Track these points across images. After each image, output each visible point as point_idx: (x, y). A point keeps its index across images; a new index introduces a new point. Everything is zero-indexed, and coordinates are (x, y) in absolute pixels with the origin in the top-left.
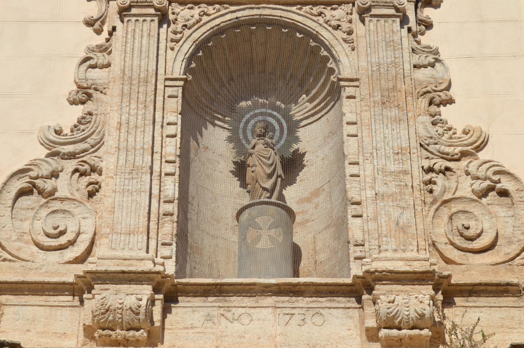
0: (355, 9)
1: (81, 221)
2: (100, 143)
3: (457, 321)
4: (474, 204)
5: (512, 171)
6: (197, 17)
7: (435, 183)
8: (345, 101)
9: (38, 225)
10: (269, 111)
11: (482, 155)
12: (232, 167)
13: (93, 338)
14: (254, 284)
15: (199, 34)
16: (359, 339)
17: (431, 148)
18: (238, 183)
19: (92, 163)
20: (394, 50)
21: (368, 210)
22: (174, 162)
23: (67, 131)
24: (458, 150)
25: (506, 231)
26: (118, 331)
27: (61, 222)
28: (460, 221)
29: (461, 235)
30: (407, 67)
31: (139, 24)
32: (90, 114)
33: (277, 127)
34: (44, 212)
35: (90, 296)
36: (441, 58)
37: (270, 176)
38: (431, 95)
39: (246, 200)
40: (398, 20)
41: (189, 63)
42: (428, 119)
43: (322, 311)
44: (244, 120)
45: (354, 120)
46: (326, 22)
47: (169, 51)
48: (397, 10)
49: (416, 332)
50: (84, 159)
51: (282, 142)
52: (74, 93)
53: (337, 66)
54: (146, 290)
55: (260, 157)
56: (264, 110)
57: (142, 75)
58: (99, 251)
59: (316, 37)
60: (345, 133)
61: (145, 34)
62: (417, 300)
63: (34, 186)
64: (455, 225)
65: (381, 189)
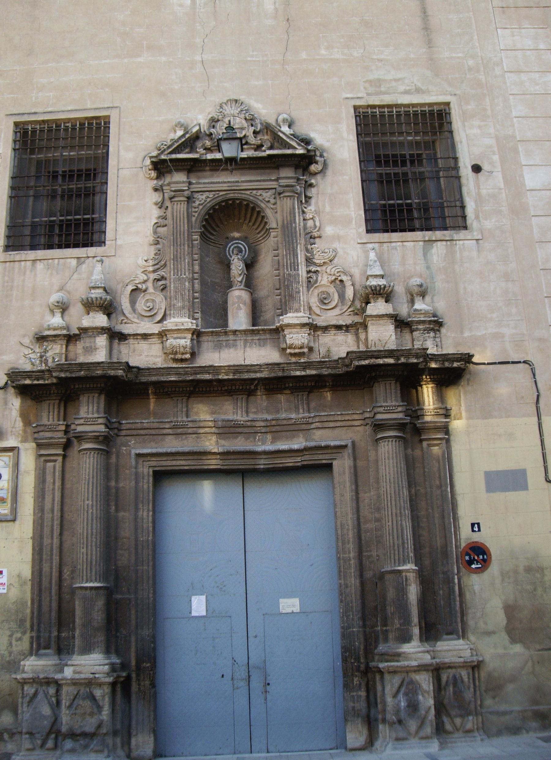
33: (243, 249)
37: (240, 275)
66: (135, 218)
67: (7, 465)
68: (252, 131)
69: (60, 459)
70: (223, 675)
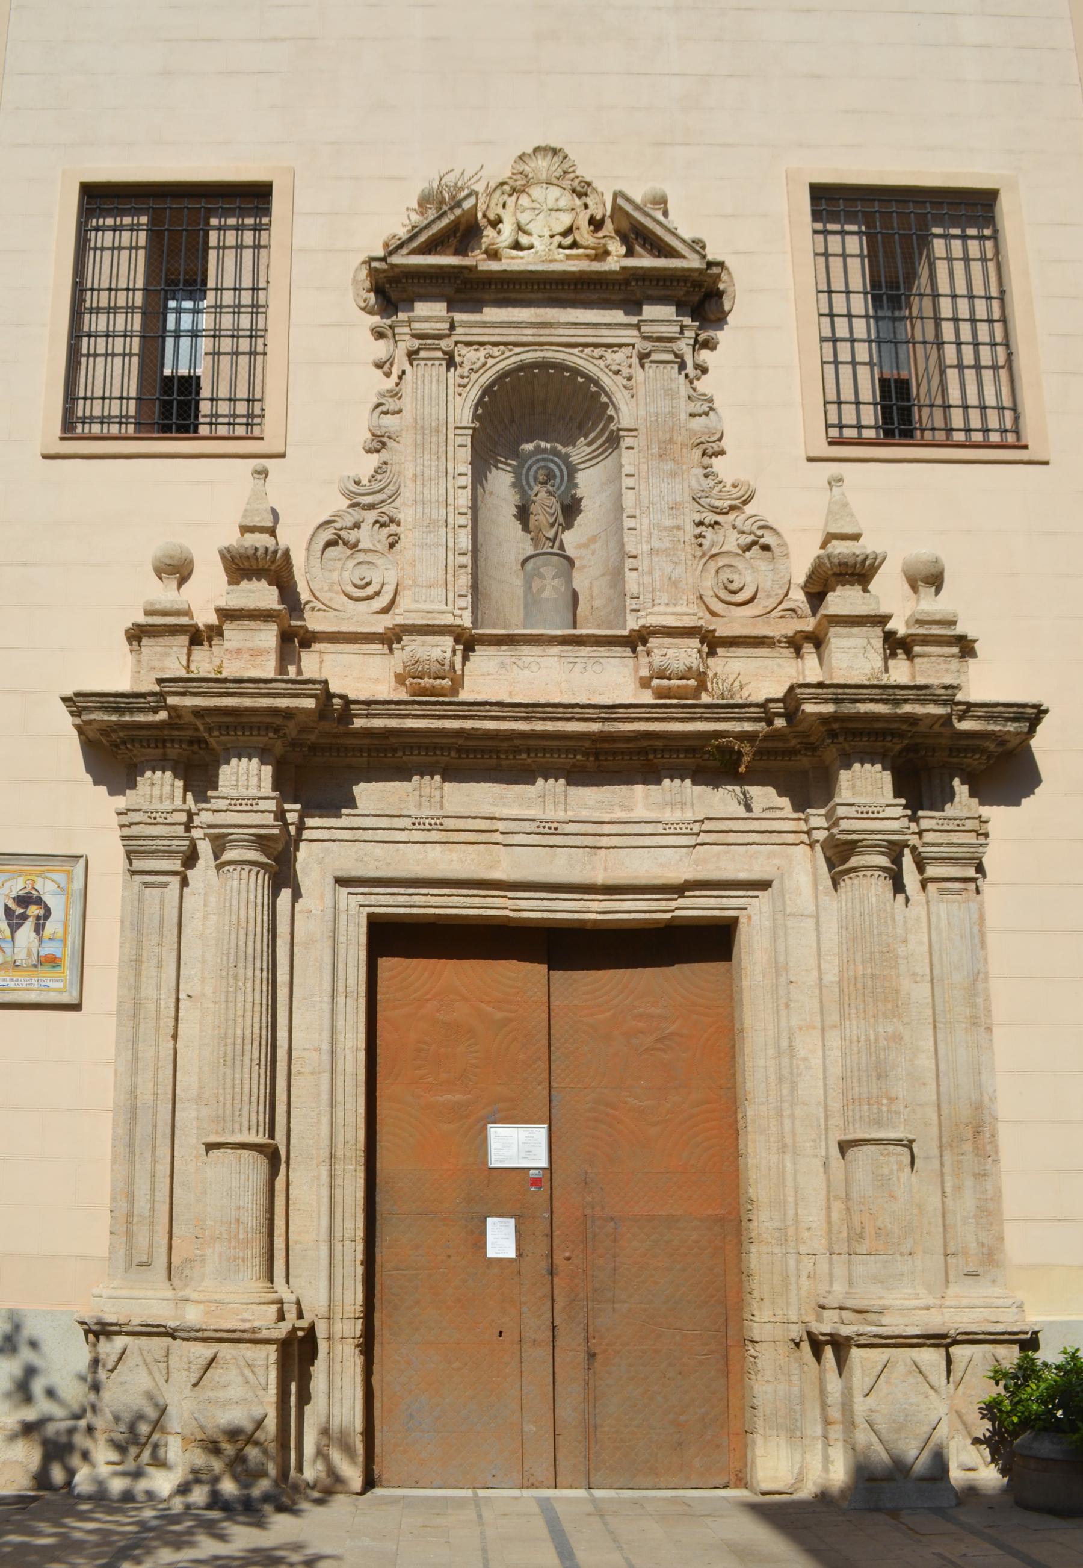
0: (635, 352)
1: (384, 573)
2: (396, 494)
3: (719, 670)
4: (738, 558)
5: (774, 527)
6: (482, 360)
7: (704, 537)
8: (624, 451)
9: (346, 575)
10: (551, 457)
11: (749, 509)
12: (514, 511)
13: (403, 684)
14: (542, 635)
15: (486, 378)
16: (633, 686)
17: (702, 501)
18: (520, 527)
19: (391, 514)
20: (672, 399)
21: (643, 564)
22: (466, 514)
23: (365, 481)
24: (729, 503)
25: (767, 584)
26: (426, 679)
27: (368, 573)
28: (725, 575)
29: (726, 588)
30: (684, 416)
31: (428, 369)
32: (386, 463)
33: (558, 473)
34: (351, 564)
35: (399, 646)
36: (715, 406)
37: (552, 525)
38: (704, 446)
39: (530, 551)
40: (676, 366)
41: (476, 409)
42: (701, 472)
43: (601, 660)
44: (527, 466)
45: (632, 473)
46: (607, 367)
47: (457, 397)
48: (676, 356)
49: (684, 682)
50: (383, 510)
51: (562, 488)
52: (369, 441)
53: (617, 413)
54: (449, 641)
55: (543, 506)
56: (545, 456)
57: (434, 424)
58: (403, 603)
59: (597, 383)
60: (624, 486)
61: (434, 380)
62: (683, 654)
63: (339, 537)
64: (720, 578)
65: (656, 544)
66: (330, 386)
67: (62, 889)
68: (587, 217)
69: (175, 881)
70: (501, 1332)
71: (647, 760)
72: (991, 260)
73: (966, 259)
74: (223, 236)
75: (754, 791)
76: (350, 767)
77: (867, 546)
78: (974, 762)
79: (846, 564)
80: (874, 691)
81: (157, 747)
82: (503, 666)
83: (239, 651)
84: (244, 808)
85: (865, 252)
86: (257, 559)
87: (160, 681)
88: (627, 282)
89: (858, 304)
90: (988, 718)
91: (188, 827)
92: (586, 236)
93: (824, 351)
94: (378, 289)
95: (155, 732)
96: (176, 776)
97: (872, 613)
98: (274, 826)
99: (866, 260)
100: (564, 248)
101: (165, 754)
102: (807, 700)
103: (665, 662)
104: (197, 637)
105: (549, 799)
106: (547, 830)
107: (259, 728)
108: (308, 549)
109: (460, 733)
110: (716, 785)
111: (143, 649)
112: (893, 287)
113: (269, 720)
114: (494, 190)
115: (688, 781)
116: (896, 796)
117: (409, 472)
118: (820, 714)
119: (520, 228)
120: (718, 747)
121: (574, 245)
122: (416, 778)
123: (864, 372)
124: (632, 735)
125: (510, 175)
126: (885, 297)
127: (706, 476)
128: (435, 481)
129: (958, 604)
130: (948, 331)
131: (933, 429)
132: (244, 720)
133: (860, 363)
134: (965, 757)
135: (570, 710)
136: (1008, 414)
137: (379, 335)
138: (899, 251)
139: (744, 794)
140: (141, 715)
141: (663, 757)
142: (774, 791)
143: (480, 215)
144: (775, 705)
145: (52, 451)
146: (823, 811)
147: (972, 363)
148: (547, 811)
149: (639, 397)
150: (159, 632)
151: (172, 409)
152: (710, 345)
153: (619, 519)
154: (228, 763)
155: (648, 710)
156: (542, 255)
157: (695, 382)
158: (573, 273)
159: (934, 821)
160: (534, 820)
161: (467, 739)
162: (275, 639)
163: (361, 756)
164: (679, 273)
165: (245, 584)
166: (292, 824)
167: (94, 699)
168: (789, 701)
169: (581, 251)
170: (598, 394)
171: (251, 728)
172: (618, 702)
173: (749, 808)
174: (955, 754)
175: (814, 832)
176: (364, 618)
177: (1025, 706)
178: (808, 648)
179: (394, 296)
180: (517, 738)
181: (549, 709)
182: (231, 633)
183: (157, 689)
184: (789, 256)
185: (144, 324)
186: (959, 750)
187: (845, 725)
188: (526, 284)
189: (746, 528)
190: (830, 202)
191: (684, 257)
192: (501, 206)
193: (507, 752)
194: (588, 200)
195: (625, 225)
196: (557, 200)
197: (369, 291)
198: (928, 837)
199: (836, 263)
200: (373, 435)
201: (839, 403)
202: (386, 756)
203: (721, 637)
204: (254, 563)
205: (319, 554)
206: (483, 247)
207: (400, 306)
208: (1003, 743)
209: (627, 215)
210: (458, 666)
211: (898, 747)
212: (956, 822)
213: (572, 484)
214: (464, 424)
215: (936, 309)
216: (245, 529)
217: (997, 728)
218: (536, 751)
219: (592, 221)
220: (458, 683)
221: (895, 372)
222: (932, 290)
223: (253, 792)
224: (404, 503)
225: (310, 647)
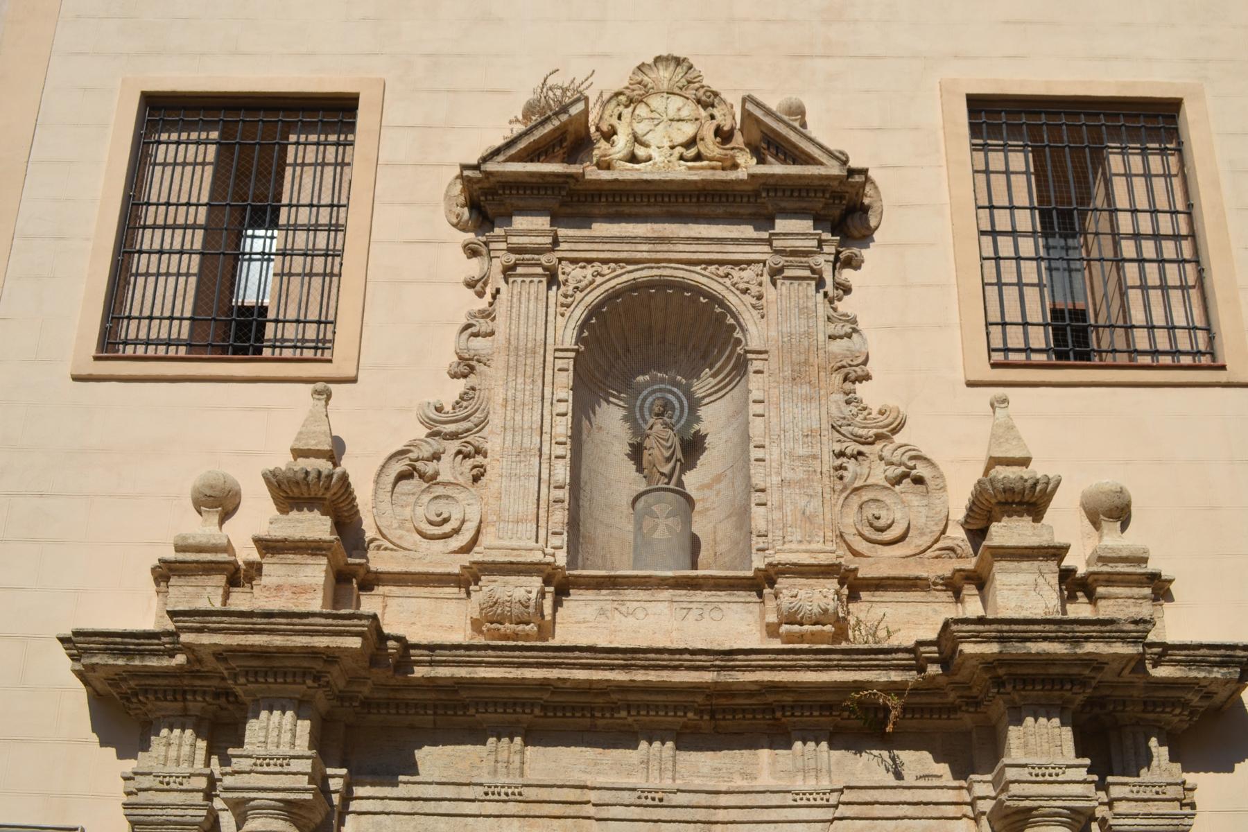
0: (766, 270)
1: (465, 508)
2: (484, 422)
3: (862, 616)
4: (887, 492)
5: (928, 456)
6: (590, 277)
7: (846, 469)
8: (751, 376)
10: (669, 387)
11: (898, 439)
12: (628, 449)
14: (650, 577)
15: (592, 297)
16: (758, 635)
17: (843, 430)
20: (808, 318)
21: (773, 498)
22: (565, 444)
23: (448, 408)
24: (873, 432)
25: (919, 520)
26: (507, 625)
27: (445, 508)
29: (871, 525)
30: (821, 337)
31: (526, 286)
32: (473, 389)
33: (677, 405)
34: (426, 498)
35: (477, 588)
36: (859, 328)
37: (668, 460)
38: (845, 371)
39: (643, 487)
40: (813, 283)
42: (842, 398)
43: (721, 606)
44: (641, 397)
46: (734, 285)
47: (559, 317)
48: (813, 271)
49: (819, 627)
51: (682, 422)
52: (455, 365)
54: (536, 582)
55: (658, 438)
57: (530, 345)
58: (485, 540)
59: (721, 303)
60: (751, 413)
61: (532, 298)
62: (820, 595)
63: (415, 468)
65: (787, 474)
66: (410, 307)
68: (713, 128)
71: (774, 719)
72: (1176, 176)
73: (1148, 175)
74: (302, 151)
75: (905, 756)
76: (412, 727)
77: (1038, 470)
78: (1175, 718)
79: (1012, 490)
80: (1048, 627)
81: (175, 700)
82: (602, 612)
83: (279, 588)
84: (272, 769)
85: (1032, 170)
86: (308, 484)
87: (173, 614)
88: (757, 194)
89: (1024, 221)
90: (1189, 663)
91: (209, 794)
92: (711, 146)
93: (985, 271)
94: (473, 204)
95: (173, 681)
96: (198, 735)
97: (1045, 544)
98: (306, 790)
99: (1033, 178)
100: (686, 161)
101: (185, 709)
102: (965, 639)
103: (796, 603)
104: (237, 576)
105: (654, 766)
106: (649, 802)
107: (294, 675)
108: (377, 482)
109: (544, 684)
110: (859, 750)
111: (170, 589)
112: (1064, 214)
113: (306, 664)
114: (609, 101)
115: (824, 745)
116: (1078, 756)
117: (499, 399)
118: (982, 655)
119: (636, 139)
120: (860, 702)
121: (698, 157)
122: (492, 740)
123: (1032, 295)
124: (755, 687)
125: (626, 84)
126: (1054, 212)
127: (848, 403)
128: (529, 411)
129: (1151, 538)
130: (1128, 249)
131: (1114, 351)
132: (277, 664)
133: (1027, 285)
134: (1163, 712)
135: (677, 657)
136: (1201, 335)
137: (472, 252)
138: (1069, 164)
139: (893, 759)
140: (155, 659)
141: (793, 715)
142: (930, 756)
143: (593, 129)
144: (928, 649)
145: (84, 372)
146: (989, 777)
147: (1158, 283)
148: (651, 779)
149: (770, 317)
150: (191, 570)
151: (233, 333)
152: (854, 263)
153: (746, 452)
154: (257, 716)
155: (773, 656)
156: (662, 165)
157: (836, 303)
158: (695, 182)
159: (1127, 789)
160: (634, 790)
161: (553, 693)
162: (323, 574)
163: (426, 714)
164: (816, 182)
165: (294, 514)
166: (336, 792)
167: (97, 639)
168: (944, 643)
169: (705, 163)
170: (724, 316)
171: (285, 674)
172: (736, 647)
173: (899, 775)
174: (1150, 708)
175: (979, 802)
176: (440, 557)
177: (1234, 647)
178: (969, 590)
179: (490, 210)
180: (614, 692)
181: (652, 656)
182: (272, 567)
183: (170, 626)
184: (944, 171)
185: (205, 242)
186: (1155, 704)
187: (1013, 670)
188: (642, 196)
189: (895, 459)
190: (991, 116)
191: (822, 164)
192: (615, 117)
193: (602, 709)
194: (715, 112)
195: (756, 136)
196: (679, 110)
197: (462, 206)
198: (1121, 807)
199: (999, 182)
200: (461, 358)
201: (1004, 324)
202: (455, 714)
203: (864, 579)
204: (304, 489)
205: (389, 487)
206: (595, 160)
207: (497, 221)
208: (1208, 696)
209: (758, 121)
210: (548, 610)
211: (1081, 697)
212: (1154, 789)
213: (694, 418)
214: (566, 346)
215: (1113, 224)
216: (298, 453)
217: (1202, 675)
218: (638, 707)
219: (718, 131)
220: (546, 630)
221: (1069, 302)
222: (1109, 205)
223: (285, 750)
224: (492, 432)
225: (372, 589)
